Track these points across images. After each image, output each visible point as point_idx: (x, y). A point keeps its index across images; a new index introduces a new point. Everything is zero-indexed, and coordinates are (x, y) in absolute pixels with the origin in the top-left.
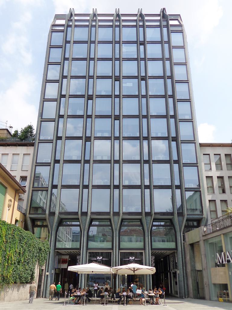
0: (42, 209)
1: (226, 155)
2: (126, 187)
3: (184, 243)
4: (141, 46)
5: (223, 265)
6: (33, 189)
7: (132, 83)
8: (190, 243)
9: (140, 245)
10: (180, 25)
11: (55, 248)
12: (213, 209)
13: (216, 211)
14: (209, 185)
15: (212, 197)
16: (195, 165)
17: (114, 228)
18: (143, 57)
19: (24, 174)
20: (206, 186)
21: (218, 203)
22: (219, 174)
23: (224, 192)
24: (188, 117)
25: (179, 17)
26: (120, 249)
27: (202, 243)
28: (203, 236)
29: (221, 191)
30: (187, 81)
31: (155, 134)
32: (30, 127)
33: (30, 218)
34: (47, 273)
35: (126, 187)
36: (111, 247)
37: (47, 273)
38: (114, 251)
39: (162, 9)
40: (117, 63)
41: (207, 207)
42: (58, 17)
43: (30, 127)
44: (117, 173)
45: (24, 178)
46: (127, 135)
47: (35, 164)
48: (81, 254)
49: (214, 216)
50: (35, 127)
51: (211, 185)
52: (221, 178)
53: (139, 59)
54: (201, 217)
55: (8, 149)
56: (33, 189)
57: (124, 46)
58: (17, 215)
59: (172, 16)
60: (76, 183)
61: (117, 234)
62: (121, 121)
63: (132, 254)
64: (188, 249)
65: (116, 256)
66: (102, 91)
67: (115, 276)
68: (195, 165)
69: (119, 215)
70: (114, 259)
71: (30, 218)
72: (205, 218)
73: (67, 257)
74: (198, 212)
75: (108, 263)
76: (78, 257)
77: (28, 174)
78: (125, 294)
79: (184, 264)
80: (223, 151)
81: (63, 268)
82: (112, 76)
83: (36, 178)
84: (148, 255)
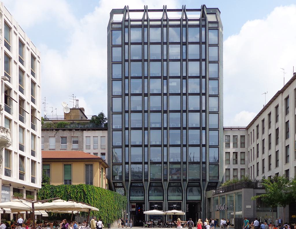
0: (100, 163)
1: (241, 136)
2: (171, 128)
3: (205, 197)
4: (183, 46)
5: (218, 210)
6: (113, 164)
7: (176, 83)
8: (208, 197)
9: (180, 198)
10: (217, 22)
11: (130, 200)
12: (228, 174)
13: (229, 176)
14: (227, 159)
15: (228, 167)
16: (217, 147)
17: (164, 189)
18: (185, 58)
19: (103, 151)
20: (224, 159)
21: (232, 170)
22: (234, 150)
23: (237, 163)
24: (216, 110)
25: (218, 11)
26: (168, 200)
27: (212, 199)
28: (213, 195)
29: (235, 163)
30: (217, 79)
31: (191, 125)
32: (102, 115)
33: (113, 182)
34: (127, 214)
35: (171, 128)
36: (162, 199)
37: (127, 214)
38: (165, 202)
39: (202, 5)
40: (165, 97)
41: (224, 174)
42: (114, 12)
43: (102, 115)
44: (165, 154)
45: (103, 154)
46: (172, 125)
47: (111, 147)
48: (146, 203)
49: (227, 179)
50: (106, 116)
51: (228, 158)
52: (236, 153)
53: (182, 77)
54: (217, 181)
55: (89, 133)
56: (113, 164)
57: (171, 47)
58: (105, 182)
59: (211, 9)
60: (140, 161)
61: (166, 192)
62: (168, 80)
63: (175, 203)
64: (207, 200)
65: (165, 204)
66: (154, 89)
67: (165, 215)
68: (217, 147)
69: (167, 181)
70: (165, 206)
71: (113, 182)
72: (220, 182)
73: (135, 204)
74: (216, 178)
75: (160, 209)
76: (143, 205)
77: (106, 151)
78: (170, 223)
79: (205, 209)
80: (239, 134)
81: (133, 211)
82: (161, 76)
83: (111, 156)
84: (184, 205)
